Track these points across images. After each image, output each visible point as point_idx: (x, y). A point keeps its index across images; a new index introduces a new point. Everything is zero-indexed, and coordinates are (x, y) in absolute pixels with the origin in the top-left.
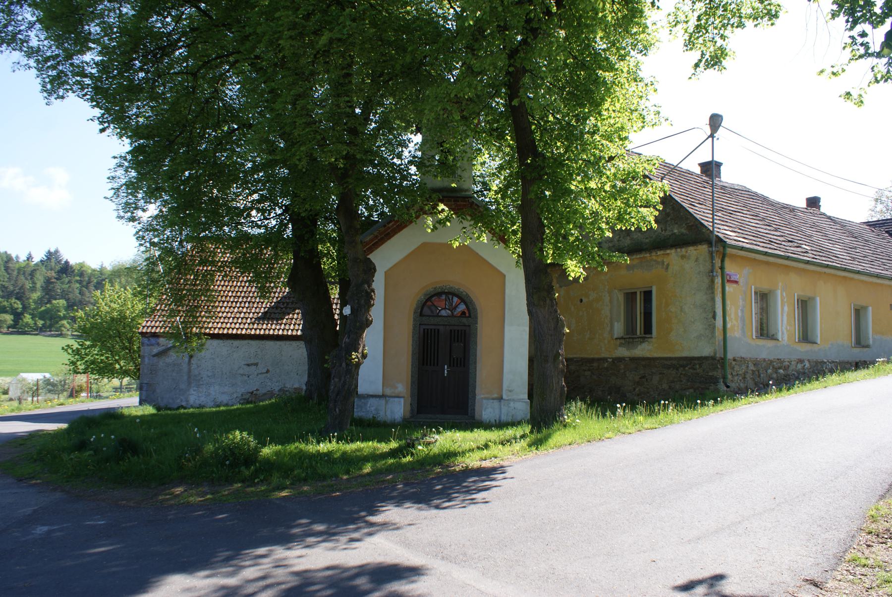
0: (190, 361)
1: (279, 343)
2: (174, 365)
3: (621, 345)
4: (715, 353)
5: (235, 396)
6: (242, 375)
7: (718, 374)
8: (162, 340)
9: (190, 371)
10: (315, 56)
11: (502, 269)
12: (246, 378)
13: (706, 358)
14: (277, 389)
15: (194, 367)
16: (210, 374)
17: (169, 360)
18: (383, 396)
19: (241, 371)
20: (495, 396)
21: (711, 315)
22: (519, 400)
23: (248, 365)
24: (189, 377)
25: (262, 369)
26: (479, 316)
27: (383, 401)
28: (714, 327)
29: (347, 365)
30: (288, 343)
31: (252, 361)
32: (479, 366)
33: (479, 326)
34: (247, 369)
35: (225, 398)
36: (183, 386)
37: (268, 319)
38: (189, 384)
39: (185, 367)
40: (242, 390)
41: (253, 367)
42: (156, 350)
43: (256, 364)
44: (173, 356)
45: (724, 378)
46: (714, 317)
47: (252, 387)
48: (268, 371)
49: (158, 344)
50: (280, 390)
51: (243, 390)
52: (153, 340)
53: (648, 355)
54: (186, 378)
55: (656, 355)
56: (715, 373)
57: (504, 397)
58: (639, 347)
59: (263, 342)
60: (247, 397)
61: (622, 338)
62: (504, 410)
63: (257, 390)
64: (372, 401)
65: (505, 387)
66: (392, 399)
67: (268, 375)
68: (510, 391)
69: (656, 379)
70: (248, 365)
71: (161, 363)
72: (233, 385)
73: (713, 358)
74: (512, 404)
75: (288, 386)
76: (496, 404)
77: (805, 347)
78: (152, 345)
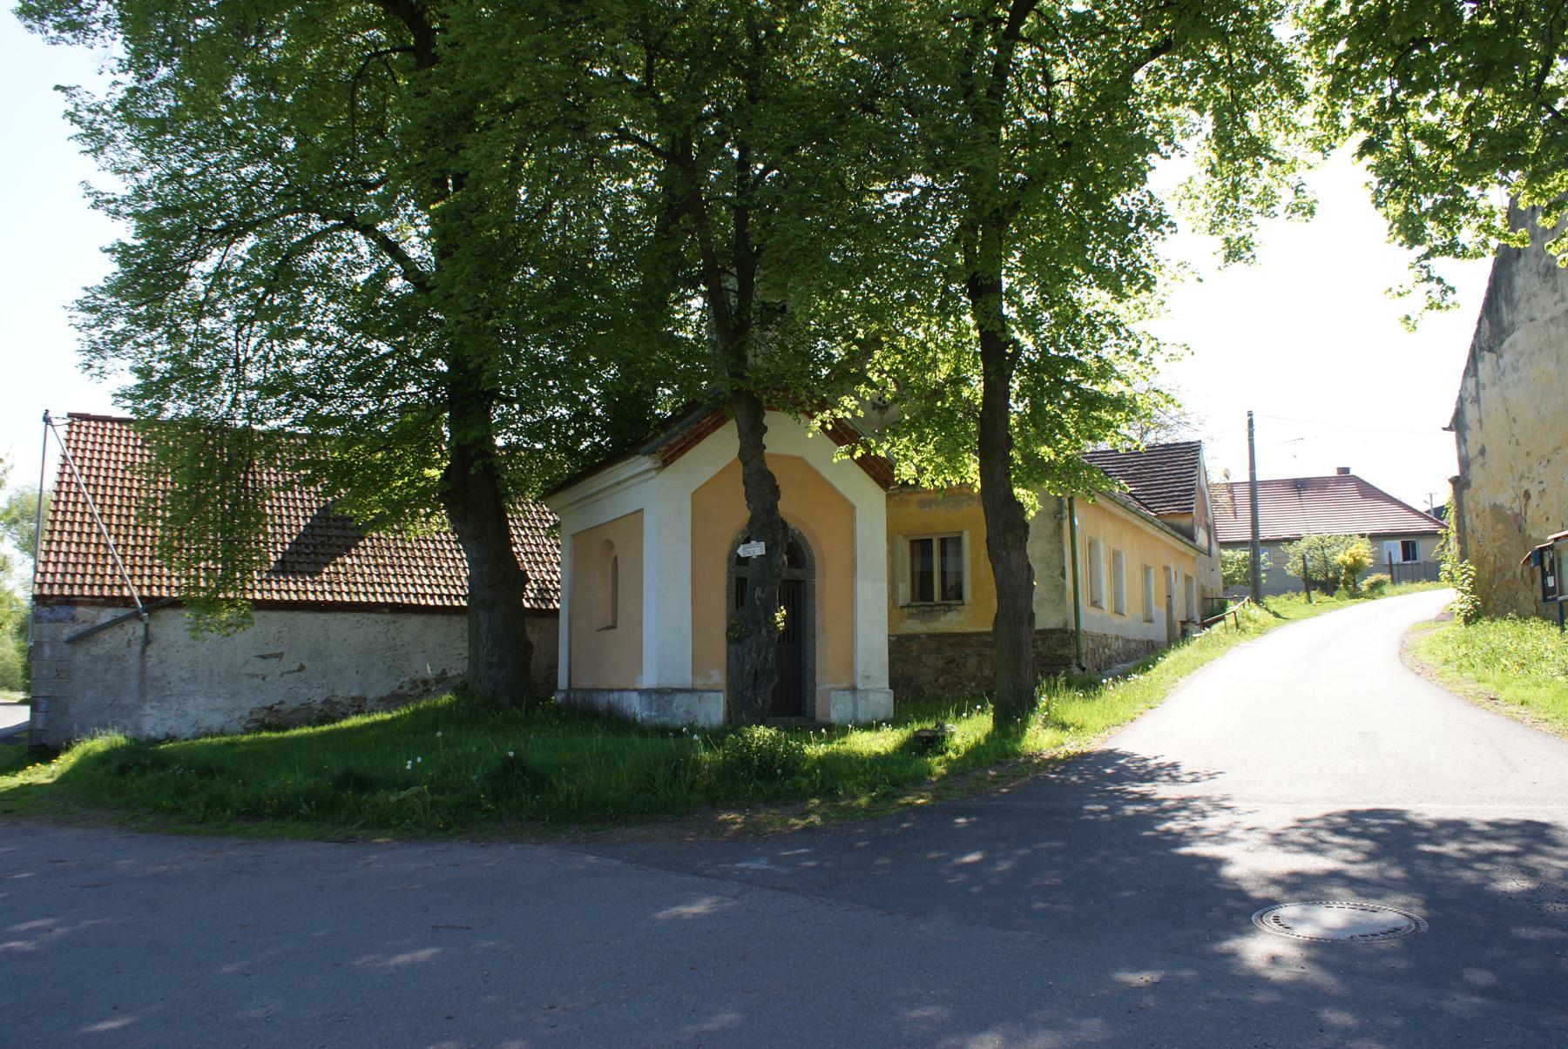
0: (143, 651)
1: (323, 617)
2: (110, 659)
3: (910, 616)
4: (1066, 624)
5: (237, 714)
6: (252, 676)
7: (1070, 652)
8: (81, 611)
9: (143, 671)
10: (557, 121)
11: (851, 498)
12: (258, 681)
13: (1052, 631)
14: (319, 700)
15: (152, 662)
16: (186, 676)
17: (96, 650)
18: (692, 691)
19: (249, 669)
20: (845, 685)
21: (1058, 572)
22: (879, 690)
23: (263, 657)
24: (143, 681)
25: (290, 663)
26: (818, 566)
27: (695, 698)
28: (1064, 588)
29: (769, 632)
30: (340, 616)
31: (271, 650)
32: (819, 641)
33: (818, 581)
34: (261, 664)
35: (215, 721)
36: (128, 700)
37: (285, 573)
38: (143, 694)
39: (133, 662)
40: (250, 703)
41: (274, 661)
42: (68, 631)
43: (280, 656)
44: (110, 641)
45: (1078, 657)
46: (1063, 575)
47: (272, 699)
48: (302, 668)
49: (73, 619)
50: (325, 702)
51: (254, 704)
52: (62, 612)
53: (958, 629)
54: (134, 683)
55: (970, 629)
56: (1067, 652)
57: (860, 686)
58: (943, 619)
59: (293, 615)
60: (261, 716)
61: (908, 606)
62: (861, 706)
63: (281, 703)
64: (679, 698)
65: (860, 669)
66: (706, 695)
67: (302, 674)
68: (867, 677)
69: (972, 663)
70: (263, 657)
71: (80, 656)
72: (233, 695)
73: (1063, 631)
74: (871, 696)
75: (340, 693)
76: (848, 696)
77: (1117, 619)
78: (60, 621)
